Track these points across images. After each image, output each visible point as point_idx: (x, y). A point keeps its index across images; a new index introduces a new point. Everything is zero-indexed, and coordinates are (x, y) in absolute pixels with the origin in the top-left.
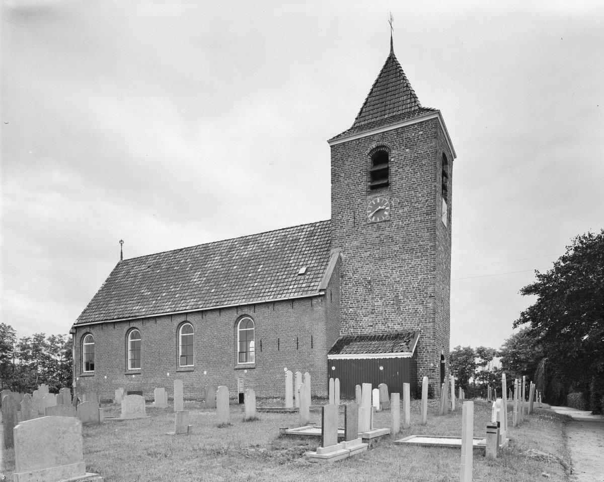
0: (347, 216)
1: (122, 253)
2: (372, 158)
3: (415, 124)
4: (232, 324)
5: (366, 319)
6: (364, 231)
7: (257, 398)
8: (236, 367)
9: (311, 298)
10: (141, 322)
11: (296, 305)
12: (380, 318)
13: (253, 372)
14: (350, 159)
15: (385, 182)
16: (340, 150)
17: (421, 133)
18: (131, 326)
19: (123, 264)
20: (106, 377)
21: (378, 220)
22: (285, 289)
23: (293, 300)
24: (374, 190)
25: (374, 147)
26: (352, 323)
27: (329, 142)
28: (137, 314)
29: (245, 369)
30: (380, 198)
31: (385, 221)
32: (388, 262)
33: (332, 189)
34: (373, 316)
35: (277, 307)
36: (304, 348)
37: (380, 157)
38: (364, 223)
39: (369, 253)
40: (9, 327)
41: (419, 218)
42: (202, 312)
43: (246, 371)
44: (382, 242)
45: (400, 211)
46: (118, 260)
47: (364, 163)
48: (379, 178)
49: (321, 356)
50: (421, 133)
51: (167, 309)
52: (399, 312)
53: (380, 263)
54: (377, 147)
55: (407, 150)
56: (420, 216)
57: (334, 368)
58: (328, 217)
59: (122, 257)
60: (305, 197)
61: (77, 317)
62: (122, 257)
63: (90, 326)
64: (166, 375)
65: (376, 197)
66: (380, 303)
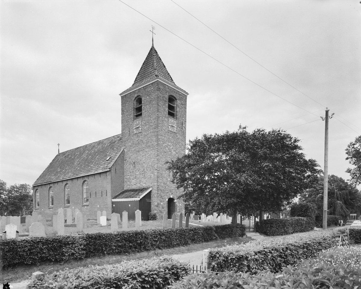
0: (127, 131)
1: (59, 150)
2: (137, 101)
3: (150, 84)
4: (81, 185)
5: (133, 181)
6: (133, 138)
7: (97, 220)
8: (36, 208)
9: (106, 172)
10: (53, 184)
11: (102, 175)
12: (138, 180)
13: (88, 207)
14: (128, 103)
15: (140, 113)
16: (125, 97)
17: (152, 88)
18: (50, 186)
19: (59, 155)
20: (43, 210)
21: (137, 132)
22: (89, 171)
23: (100, 173)
24: (137, 117)
25: (136, 96)
26: (129, 183)
27: (120, 95)
28: (52, 180)
29: (85, 206)
30: (138, 121)
31: (140, 133)
32: (141, 153)
33: (122, 117)
34: (136, 179)
35: (96, 176)
36: (104, 196)
37: (139, 100)
38: (133, 134)
39: (134, 148)
40: (28, 185)
41: (152, 131)
42: (72, 179)
43: (86, 207)
44: (139, 143)
45: (145, 127)
46: (57, 153)
47: (132, 104)
48: (139, 112)
49: (109, 200)
50: (152, 88)
51: (61, 179)
52: (145, 177)
53: (138, 153)
54: (137, 96)
55: (148, 97)
56: (152, 130)
57: (114, 206)
58: (120, 132)
59: (59, 152)
60: (109, 124)
61: (34, 182)
62: (59, 152)
63: (38, 186)
64: (207, 195)
65: (137, 121)
66: (138, 173)
